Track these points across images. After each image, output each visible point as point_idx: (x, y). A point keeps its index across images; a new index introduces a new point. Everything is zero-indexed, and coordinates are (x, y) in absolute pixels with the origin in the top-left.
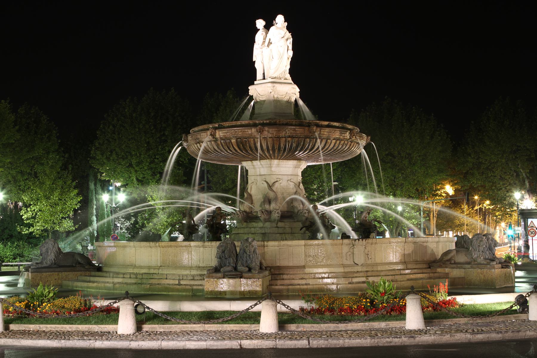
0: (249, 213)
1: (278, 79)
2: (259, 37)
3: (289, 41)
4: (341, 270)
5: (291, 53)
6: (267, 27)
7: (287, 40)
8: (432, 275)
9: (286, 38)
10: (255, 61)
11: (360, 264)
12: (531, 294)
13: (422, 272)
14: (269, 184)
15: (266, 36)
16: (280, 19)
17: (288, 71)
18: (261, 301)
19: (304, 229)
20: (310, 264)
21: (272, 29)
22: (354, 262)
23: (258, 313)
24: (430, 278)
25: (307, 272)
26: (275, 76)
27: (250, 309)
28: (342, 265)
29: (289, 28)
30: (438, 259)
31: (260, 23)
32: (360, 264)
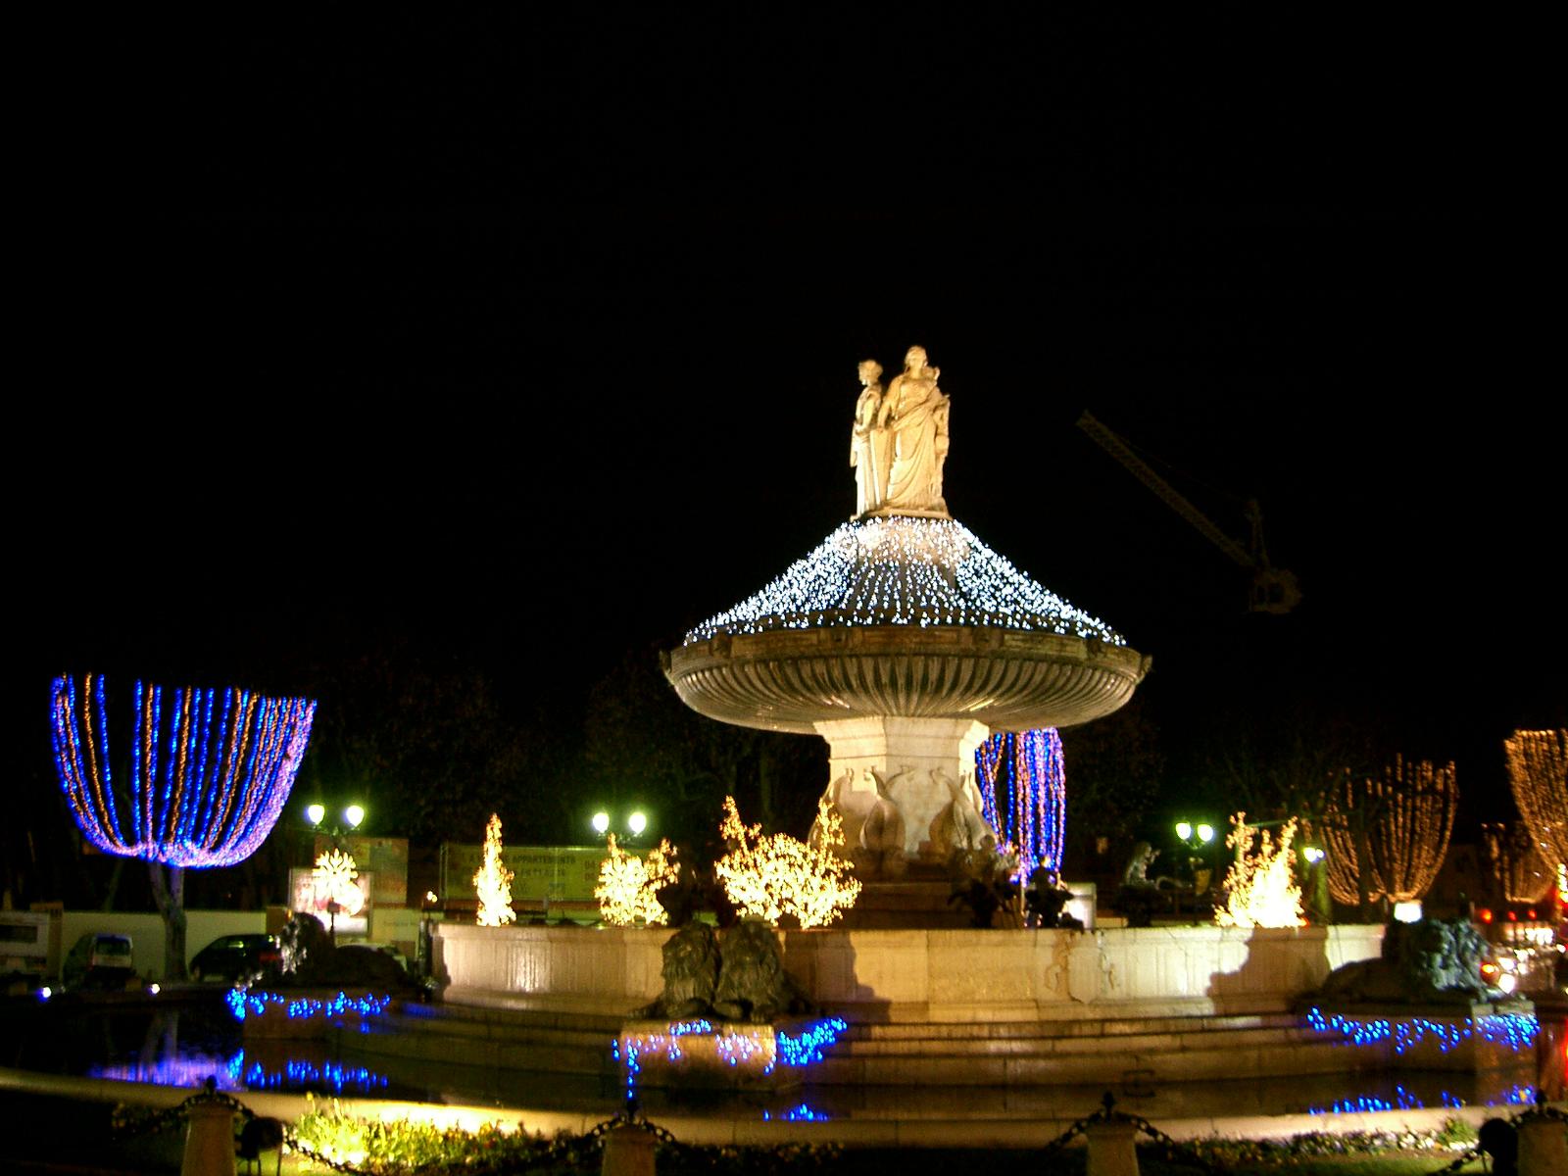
0: (1501, 917)
1: (909, 508)
2: (865, 408)
3: (939, 413)
4: (1031, 1015)
5: (944, 443)
6: (884, 382)
7: (935, 409)
8: (1294, 1033)
9: (931, 404)
10: (855, 468)
11: (1086, 1003)
12: (593, 1131)
13: (1163, 1030)
14: (882, 782)
15: (882, 402)
16: (916, 358)
17: (940, 487)
18: (232, 1102)
19: (958, 900)
20: (942, 996)
21: (895, 384)
22: (1069, 994)
23: (1319, 1111)
24: (1291, 1043)
25: (932, 1020)
26: (901, 503)
27: (608, 1123)
28: (1036, 1001)
29: (943, 385)
30: (1320, 985)
31: (868, 371)
32: (1086, 1003)
